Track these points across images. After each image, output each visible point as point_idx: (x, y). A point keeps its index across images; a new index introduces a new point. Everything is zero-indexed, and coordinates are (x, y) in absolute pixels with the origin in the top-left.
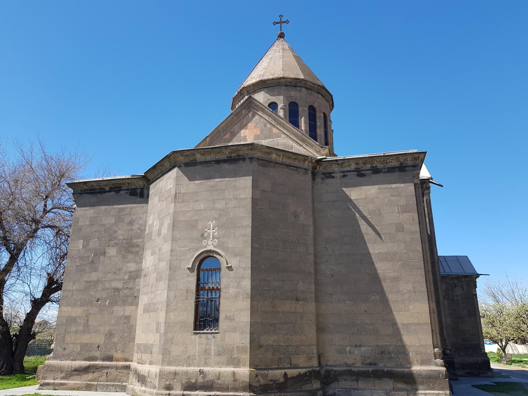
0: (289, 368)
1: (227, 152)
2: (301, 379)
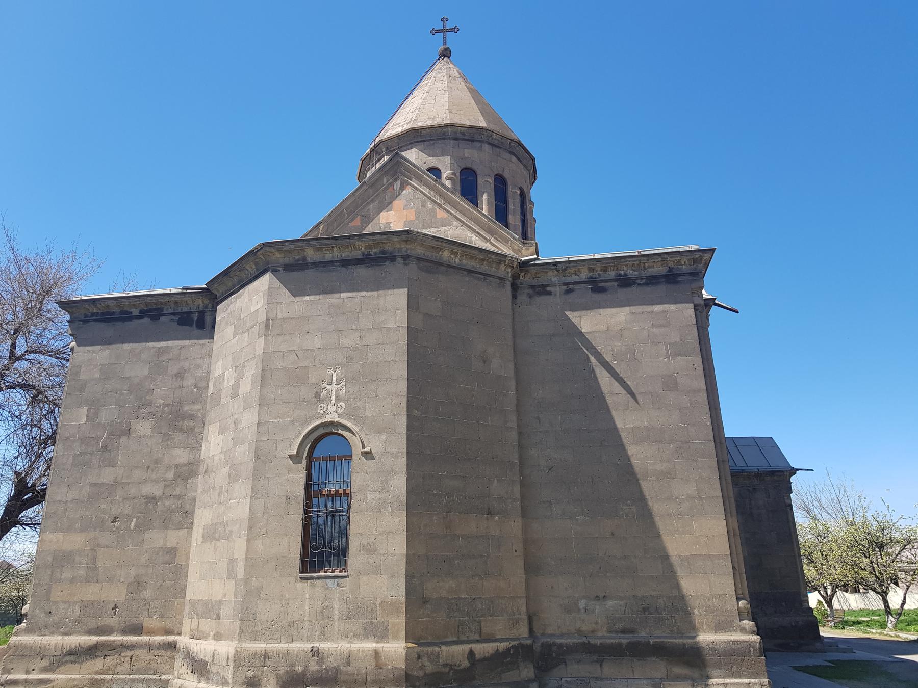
0: (478, 641)
1: (362, 246)
2: (499, 660)
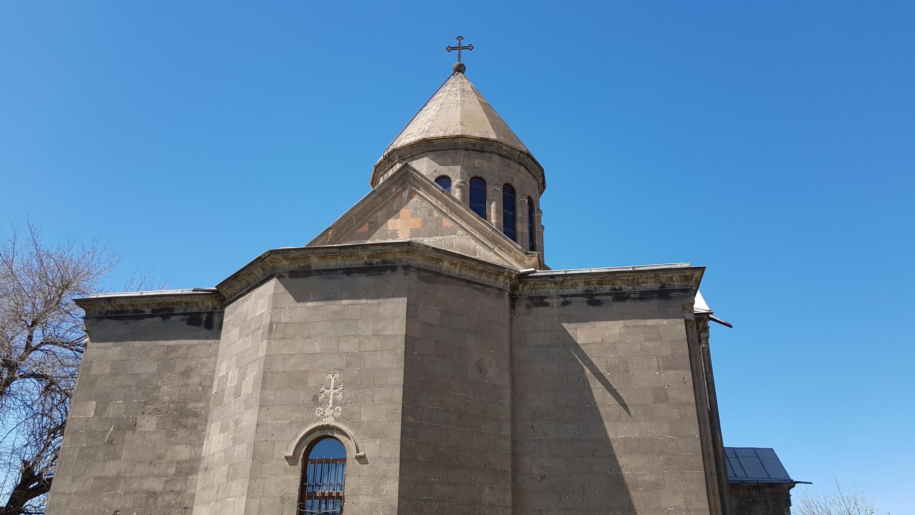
1: (365, 255)
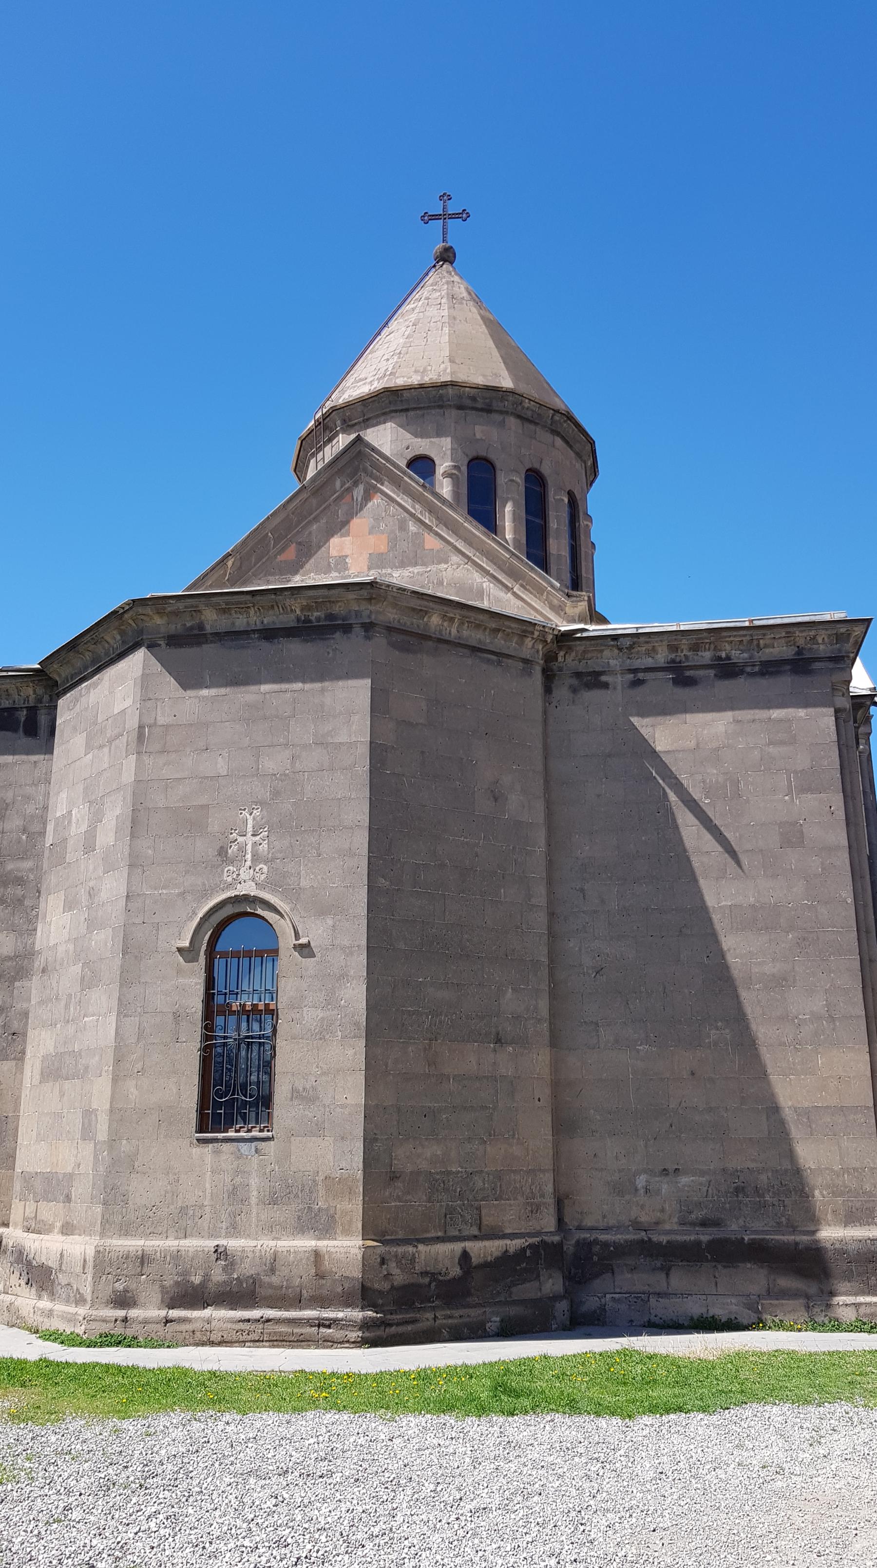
0: (475, 1238)
1: (297, 605)
